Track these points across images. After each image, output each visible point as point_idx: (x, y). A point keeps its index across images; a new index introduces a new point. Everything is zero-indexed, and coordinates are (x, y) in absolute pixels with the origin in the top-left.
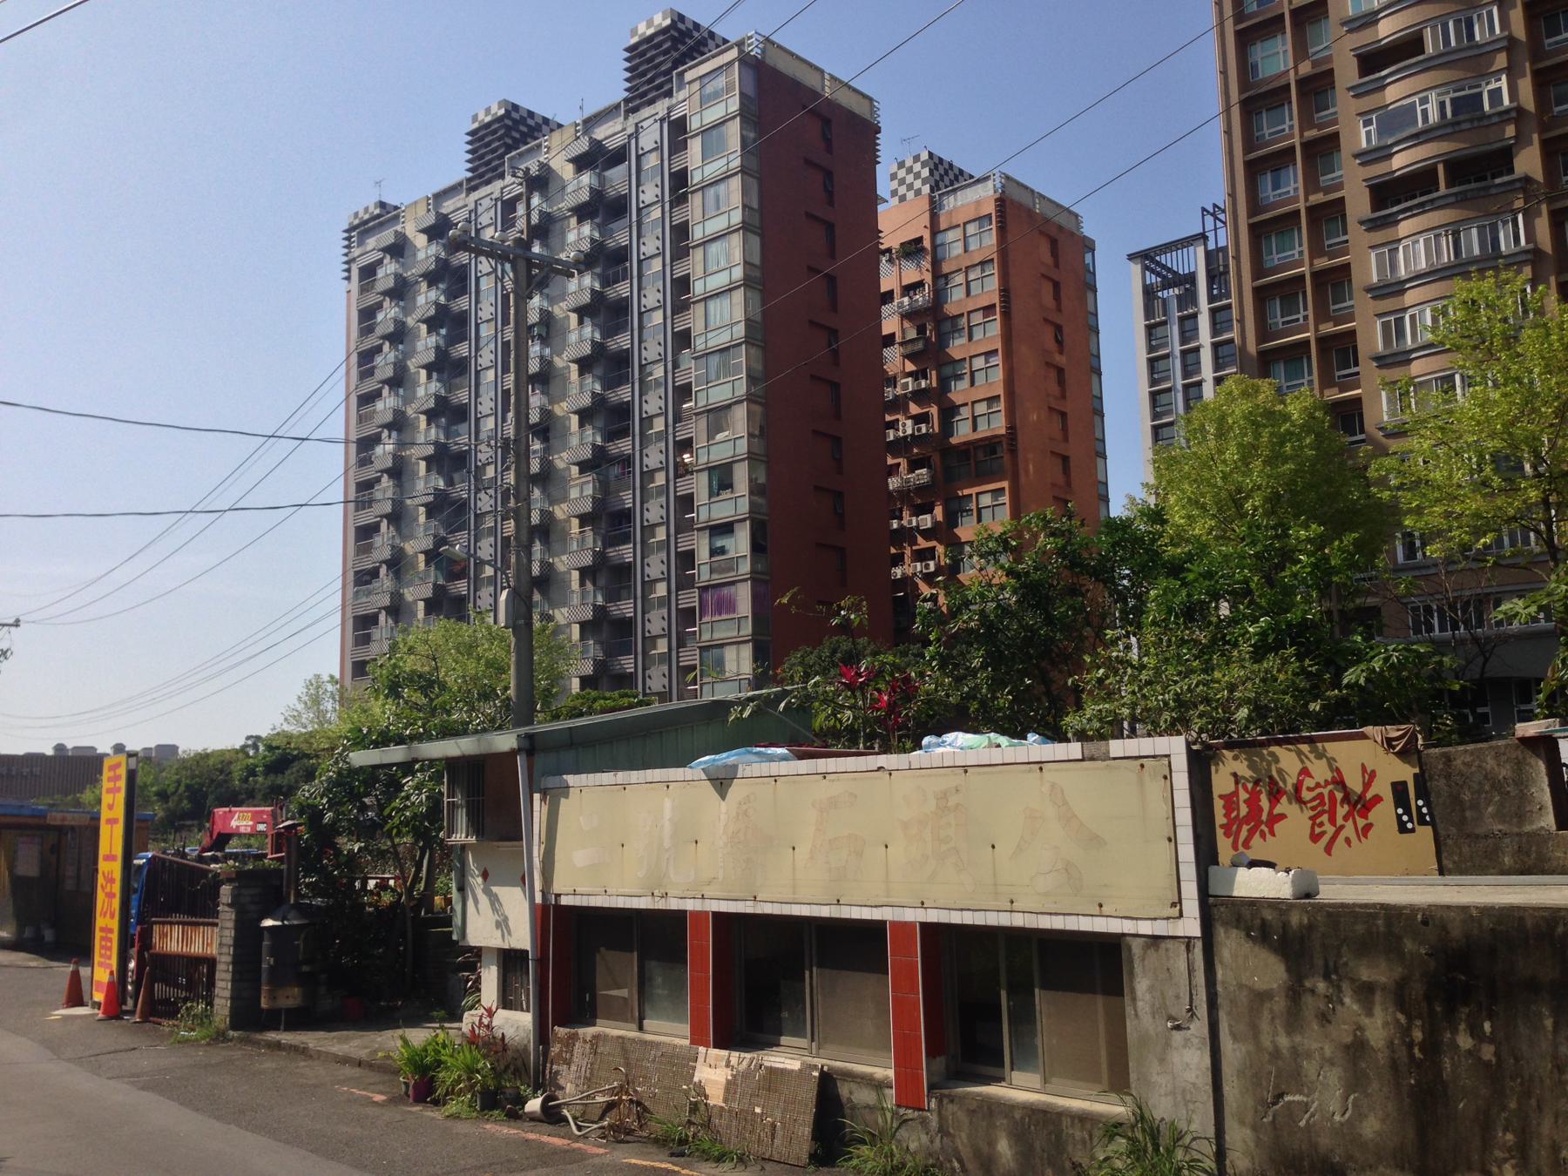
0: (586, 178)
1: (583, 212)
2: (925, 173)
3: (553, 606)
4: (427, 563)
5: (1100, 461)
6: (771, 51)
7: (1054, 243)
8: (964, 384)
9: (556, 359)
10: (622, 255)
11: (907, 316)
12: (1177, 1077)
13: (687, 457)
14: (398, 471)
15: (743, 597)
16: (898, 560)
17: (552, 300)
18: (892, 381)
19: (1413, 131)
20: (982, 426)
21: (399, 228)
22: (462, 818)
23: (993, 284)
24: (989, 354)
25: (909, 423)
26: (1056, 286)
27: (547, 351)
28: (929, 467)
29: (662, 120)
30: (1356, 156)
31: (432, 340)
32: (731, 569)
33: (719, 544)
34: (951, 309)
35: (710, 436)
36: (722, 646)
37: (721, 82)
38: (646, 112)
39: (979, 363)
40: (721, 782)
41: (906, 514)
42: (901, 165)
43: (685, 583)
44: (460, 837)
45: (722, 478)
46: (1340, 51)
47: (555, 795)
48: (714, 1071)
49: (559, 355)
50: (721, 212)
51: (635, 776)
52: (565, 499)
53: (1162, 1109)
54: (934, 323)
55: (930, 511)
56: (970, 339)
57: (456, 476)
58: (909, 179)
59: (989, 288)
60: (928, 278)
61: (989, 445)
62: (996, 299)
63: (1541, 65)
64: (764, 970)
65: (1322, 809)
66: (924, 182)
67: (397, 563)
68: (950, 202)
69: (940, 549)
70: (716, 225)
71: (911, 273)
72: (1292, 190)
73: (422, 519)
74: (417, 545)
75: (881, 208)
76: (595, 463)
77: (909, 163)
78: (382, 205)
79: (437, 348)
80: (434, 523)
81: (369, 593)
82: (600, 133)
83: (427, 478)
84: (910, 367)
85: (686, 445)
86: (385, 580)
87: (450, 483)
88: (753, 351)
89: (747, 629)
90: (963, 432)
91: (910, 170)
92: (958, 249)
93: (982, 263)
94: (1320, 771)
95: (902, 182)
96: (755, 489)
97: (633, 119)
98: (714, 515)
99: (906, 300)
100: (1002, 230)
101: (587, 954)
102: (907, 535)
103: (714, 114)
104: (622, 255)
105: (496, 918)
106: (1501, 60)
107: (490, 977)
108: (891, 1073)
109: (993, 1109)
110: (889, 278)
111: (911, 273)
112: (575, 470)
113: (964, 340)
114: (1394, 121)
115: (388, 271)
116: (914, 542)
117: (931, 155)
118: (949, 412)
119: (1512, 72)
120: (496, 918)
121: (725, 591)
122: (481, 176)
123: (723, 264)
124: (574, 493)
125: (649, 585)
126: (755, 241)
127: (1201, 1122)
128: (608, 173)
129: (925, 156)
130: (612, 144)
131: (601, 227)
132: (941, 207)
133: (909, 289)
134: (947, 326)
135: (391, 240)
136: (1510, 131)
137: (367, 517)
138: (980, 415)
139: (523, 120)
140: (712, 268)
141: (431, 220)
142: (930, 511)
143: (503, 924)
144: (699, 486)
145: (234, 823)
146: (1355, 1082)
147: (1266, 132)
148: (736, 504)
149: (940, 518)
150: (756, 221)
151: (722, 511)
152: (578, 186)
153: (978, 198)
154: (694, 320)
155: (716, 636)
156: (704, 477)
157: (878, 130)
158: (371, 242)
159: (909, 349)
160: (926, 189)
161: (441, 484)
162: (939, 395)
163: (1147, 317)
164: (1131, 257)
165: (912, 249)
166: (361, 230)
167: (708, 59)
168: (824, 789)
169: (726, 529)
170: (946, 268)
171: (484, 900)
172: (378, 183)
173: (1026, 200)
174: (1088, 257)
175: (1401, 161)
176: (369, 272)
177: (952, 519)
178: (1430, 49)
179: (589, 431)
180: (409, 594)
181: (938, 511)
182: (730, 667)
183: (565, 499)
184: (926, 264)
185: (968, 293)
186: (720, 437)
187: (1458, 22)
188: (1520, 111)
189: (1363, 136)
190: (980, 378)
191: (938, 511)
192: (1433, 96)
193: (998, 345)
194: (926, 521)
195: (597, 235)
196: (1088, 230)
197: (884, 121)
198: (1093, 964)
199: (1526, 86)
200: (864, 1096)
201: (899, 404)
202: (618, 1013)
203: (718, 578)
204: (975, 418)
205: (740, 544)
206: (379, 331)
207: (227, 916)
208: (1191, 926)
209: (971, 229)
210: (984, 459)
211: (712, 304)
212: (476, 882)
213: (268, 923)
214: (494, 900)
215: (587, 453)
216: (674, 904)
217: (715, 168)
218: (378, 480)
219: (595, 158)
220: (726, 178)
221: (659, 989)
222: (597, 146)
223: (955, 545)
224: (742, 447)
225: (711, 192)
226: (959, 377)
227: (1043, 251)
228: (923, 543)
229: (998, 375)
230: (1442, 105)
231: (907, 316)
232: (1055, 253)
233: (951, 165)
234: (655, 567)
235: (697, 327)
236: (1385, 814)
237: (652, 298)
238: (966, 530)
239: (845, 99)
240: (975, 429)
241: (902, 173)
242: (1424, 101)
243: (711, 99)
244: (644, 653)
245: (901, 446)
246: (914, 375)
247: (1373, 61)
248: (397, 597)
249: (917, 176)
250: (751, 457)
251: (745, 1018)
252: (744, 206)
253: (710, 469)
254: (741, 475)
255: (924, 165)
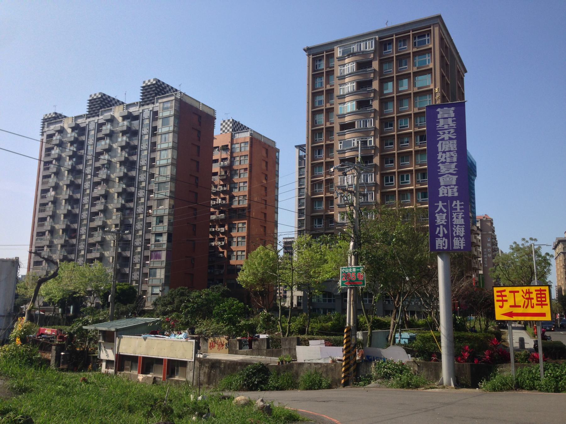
0: (126, 123)
1: (124, 133)
2: (231, 125)
3: (104, 250)
4: (63, 233)
5: (276, 214)
6: (185, 97)
7: (267, 150)
8: (237, 190)
9: (112, 175)
10: (135, 147)
11: (223, 167)
12: (190, 376)
13: (150, 211)
14: (55, 202)
15: (164, 255)
16: (213, 240)
17: (112, 157)
18: (216, 186)
19: (351, 147)
20: (241, 203)
21: (62, 125)
22: (101, 338)
23: (247, 162)
24: (245, 182)
25: (220, 200)
26: (267, 163)
27: (109, 172)
28: (225, 214)
29: (151, 111)
30: (338, 151)
31: (70, 163)
32: (160, 246)
33: (158, 239)
34: (235, 167)
35: (158, 207)
36: (156, 268)
37: (169, 105)
38: (146, 107)
39: (242, 185)
40: (145, 339)
41: (217, 227)
42: (224, 121)
43: (147, 248)
44: (100, 341)
45: (160, 220)
46: (336, 124)
47: (120, 338)
48: (141, 377)
49: (113, 174)
50: (166, 141)
51: (133, 337)
52: (111, 218)
53: (188, 379)
54: (230, 172)
55: (224, 227)
56: (240, 177)
57: (75, 206)
58: (226, 126)
59: (246, 163)
60: (229, 157)
61: (243, 209)
62: (248, 167)
63: (382, 135)
64: (148, 364)
65: (219, 345)
66: (230, 128)
67: (52, 231)
68: (237, 136)
69: (226, 238)
70: (164, 146)
71: (224, 155)
72: (323, 158)
73: (62, 218)
74: (60, 226)
75: (214, 140)
76: (122, 209)
77: (226, 121)
78: (56, 113)
79: (72, 165)
80: (66, 220)
81: (42, 239)
82: (132, 110)
83: (65, 206)
84: (222, 183)
85: (150, 207)
86: (47, 236)
87: (73, 208)
88: (172, 183)
89: (164, 265)
90: (235, 205)
91: (226, 123)
92: (238, 150)
93: (245, 156)
94: (220, 341)
95: (224, 126)
96: (170, 224)
97: (142, 108)
98: (157, 230)
99: (222, 163)
100: (251, 147)
101: (122, 362)
102: (216, 233)
103: (166, 114)
104: (135, 147)
105: (107, 354)
106: (372, 133)
107: (104, 364)
108: (162, 377)
109: (172, 380)
110: (217, 155)
111: (224, 155)
112: (115, 210)
113: (238, 177)
114: (347, 143)
115: (57, 138)
116: (219, 235)
117: (233, 120)
118: (232, 197)
119: (375, 136)
120: (107, 354)
121: (158, 253)
122: (91, 114)
123: (165, 157)
124: (114, 217)
125: (135, 247)
126: (176, 152)
127: (191, 381)
128: (133, 122)
129: (231, 120)
130: (135, 114)
131: (129, 138)
132: (235, 137)
133: (224, 160)
134: (233, 172)
135: (59, 129)
136: (373, 152)
137: (43, 215)
138: (241, 197)
139: (106, 99)
140: (162, 158)
141: (73, 125)
142: (224, 227)
143: (107, 355)
144: (154, 220)
145: (46, 331)
146: (204, 376)
147: (318, 139)
148: (164, 228)
149: (227, 229)
150: (176, 145)
151: (160, 229)
152: (123, 125)
153: (244, 136)
154: (157, 155)
155: (155, 265)
156: (155, 219)
157: (215, 119)
158: (52, 127)
159: (222, 178)
160: (231, 130)
161: (70, 208)
162: (229, 192)
163: (299, 166)
164: (296, 146)
165: (225, 148)
166: (48, 121)
167: (167, 96)
168: (158, 341)
169: (160, 235)
170: (235, 155)
171: (104, 351)
172: (55, 106)
173: (259, 138)
174: (277, 154)
175: (348, 155)
176: (50, 136)
177: (230, 230)
178: (356, 127)
179: (120, 198)
180: (56, 241)
181: (226, 227)
182: (158, 276)
183: (111, 218)
184: (229, 153)
185: (240, 164)
186: (160, 207)
187: (363, 121)
188: (376, 147)
189: (338, 146)
190: (241, 189)
191: (226, 227)
192: (356, 139)
193: (248, 180)
194: (223, 230)
195: (128, 140)
196: (277, 146)
197: (217, 116)
198: (184, 364)
199: (378, 140)
200: (159, 380)
201: (217, 194)
202: (127, 370)
203: (156, 249)
204: (239, 201)
205: (164, 239)
206: (52, 157)
207: (54, 353)
208: (193, 360)
209: (243, 145)
210: (240, 213)
211: (161, 169)
212: (103, 348)
213: (62, 353)
214: (106, 351)
215: (119, 206)
216: (137, 355)
217: (165, 129)
218: (47, 204)
219: (129, 117)
220: (168, 133)
221: (134, 367)
222: (130, 113)
223: (231, 238)
224: (167, 212)
225: (163, 136)
226: (236, 188)
227: (264, 153)
228: (221, 236)
229: (247, 189)
230: (358, 142)
231: (223, 167)
232: (267, 153)
233: (239, 123)
234: (138, 242)
235: (159, 142)
236: (225, 346)
237: (144, 147)
238: (234, 233)
239: (206, 110)
240: (239, 204)
241: (224, 124)
242: (354, 140)
243: (166, 108)
244: (132, 268)
245: (216, 206)
246: (223, 186)
247: (344, 127)
248: (51, 242)
249: (229, 125)
250: (169, 214)
251: (145, 370)
252: (173, 142)
253: (157, 217)
254: (166, 219)
255: (231, 123)
